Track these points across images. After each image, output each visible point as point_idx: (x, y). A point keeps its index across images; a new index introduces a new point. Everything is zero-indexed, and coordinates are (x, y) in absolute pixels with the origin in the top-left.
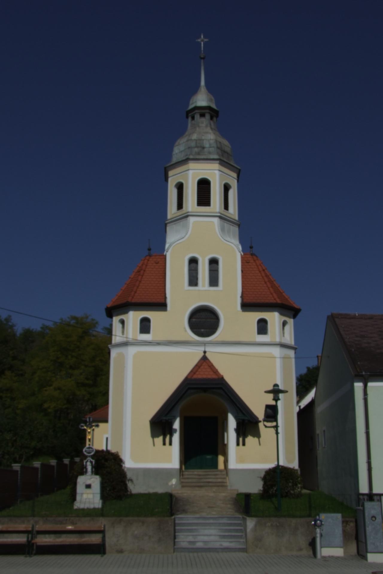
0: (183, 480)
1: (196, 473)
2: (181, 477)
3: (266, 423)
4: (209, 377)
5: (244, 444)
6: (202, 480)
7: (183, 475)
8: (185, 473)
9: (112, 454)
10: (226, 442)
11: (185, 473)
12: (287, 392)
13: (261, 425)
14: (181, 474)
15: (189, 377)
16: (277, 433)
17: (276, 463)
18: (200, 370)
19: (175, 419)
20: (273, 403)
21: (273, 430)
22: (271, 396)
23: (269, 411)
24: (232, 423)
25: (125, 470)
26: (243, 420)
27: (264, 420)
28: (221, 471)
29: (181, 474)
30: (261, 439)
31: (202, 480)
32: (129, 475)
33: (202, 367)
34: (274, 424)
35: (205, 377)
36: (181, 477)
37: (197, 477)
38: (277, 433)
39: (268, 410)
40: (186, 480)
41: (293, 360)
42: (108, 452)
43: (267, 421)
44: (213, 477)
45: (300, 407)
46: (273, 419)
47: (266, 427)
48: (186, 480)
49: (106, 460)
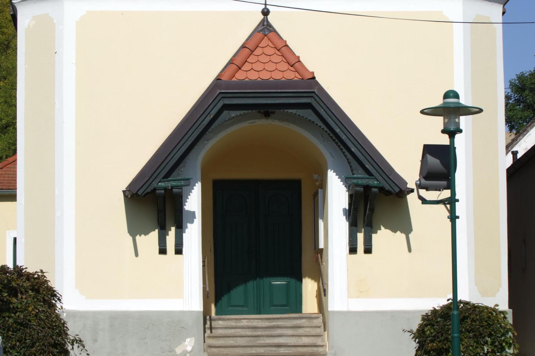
0: (210, 341)
1: (244, 323)
2: (208, 331)
3: (423, 193)
4: (278, 76)
5: (368, 250)
6: (262, 341)
7: (211, 328)
8: (214, 324)
9: (29, 277)
10: (321, 246)
11: (214, 324)
12: (481, 111)
13: (412, 199)
14: (208, 326)
15: (224, 78)
16: (453, 218)
17: (451, 296)
18: (251, 59)
19: (189, 184)
20: (444, 140)
21: (442, 211)
22: (439, 122)
23: (434, 161)
24: (512, 337)
25: (64, 316)
26: (367, 188)
27: (420, 186)
28: (310, 317)
29: (208, 326)
30: (410, 236)
31: (262, 341)
32: (73, 330)
33: (258, 51)
34: (446, 194)
35: (265, 76)
36: (208, 331)
37: (249, 332)
38: (453, 218)
39: (431, 159)
40: (221, 342)
41: (499, 28)
42: (18, 271)
43: (427, 189)
44: (290, 332)
45: (515, 154)
46: (444, 183)
47: (424, 201)
48: (221, 342)
49: (14, 292)
